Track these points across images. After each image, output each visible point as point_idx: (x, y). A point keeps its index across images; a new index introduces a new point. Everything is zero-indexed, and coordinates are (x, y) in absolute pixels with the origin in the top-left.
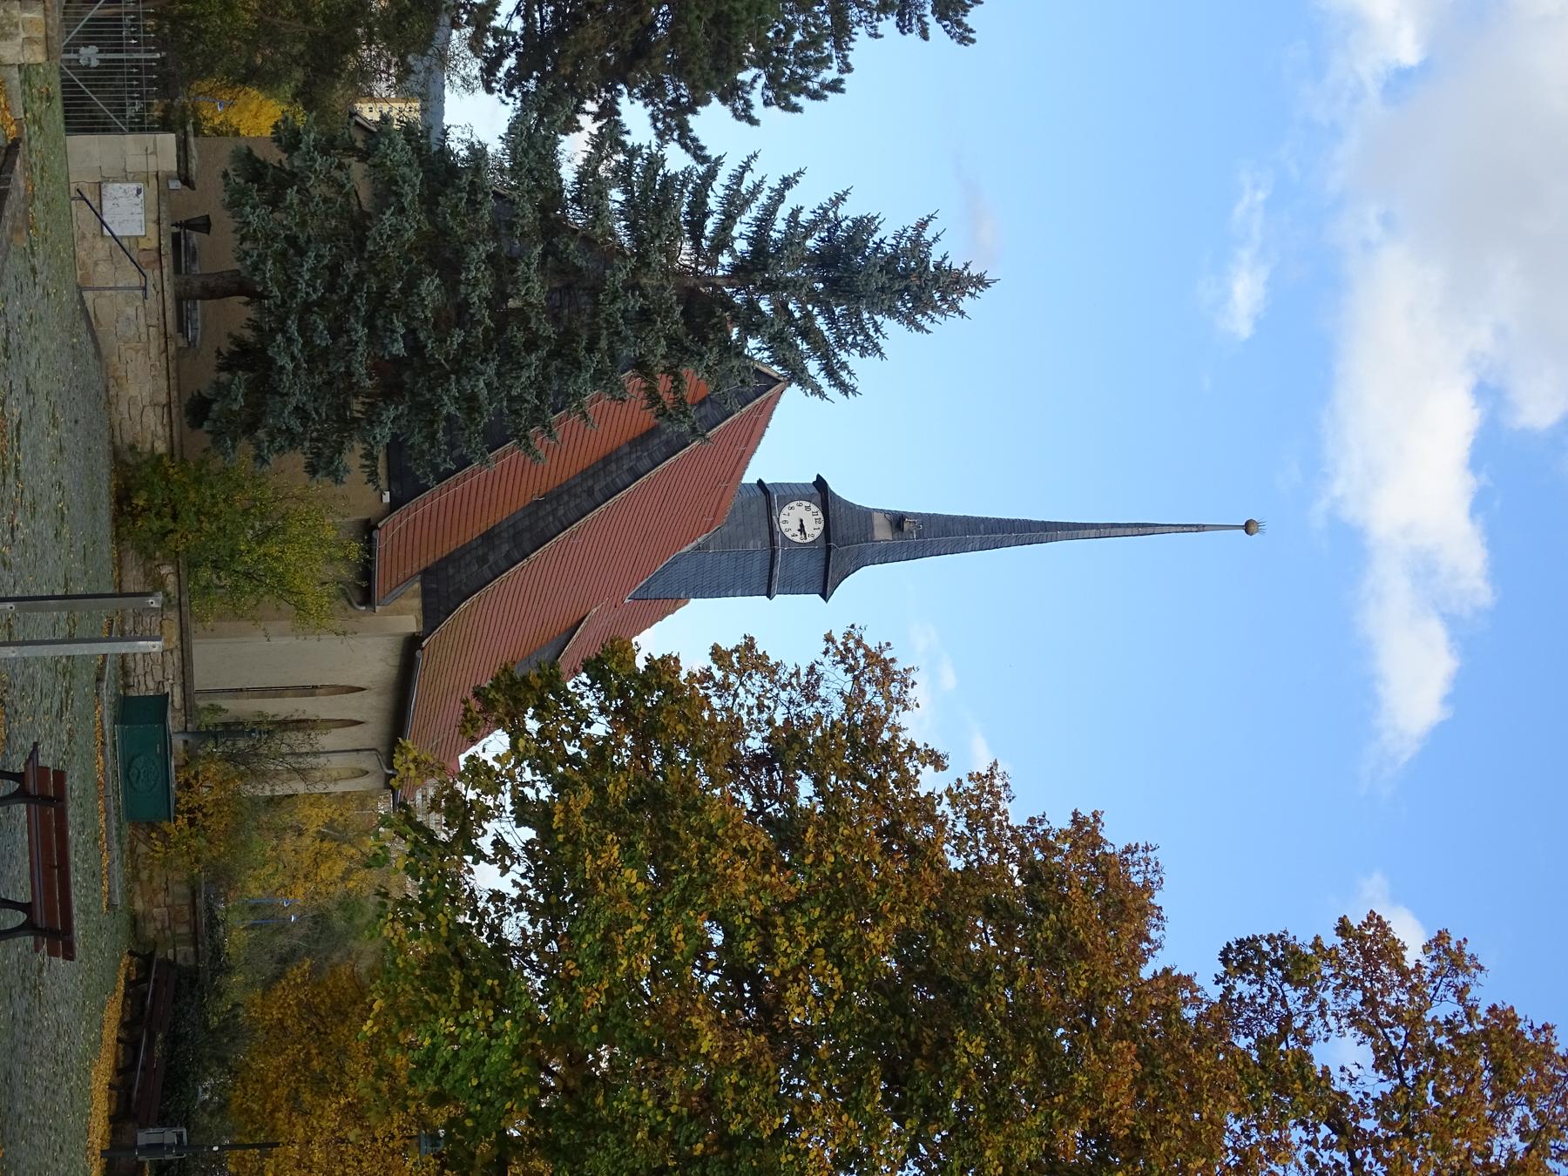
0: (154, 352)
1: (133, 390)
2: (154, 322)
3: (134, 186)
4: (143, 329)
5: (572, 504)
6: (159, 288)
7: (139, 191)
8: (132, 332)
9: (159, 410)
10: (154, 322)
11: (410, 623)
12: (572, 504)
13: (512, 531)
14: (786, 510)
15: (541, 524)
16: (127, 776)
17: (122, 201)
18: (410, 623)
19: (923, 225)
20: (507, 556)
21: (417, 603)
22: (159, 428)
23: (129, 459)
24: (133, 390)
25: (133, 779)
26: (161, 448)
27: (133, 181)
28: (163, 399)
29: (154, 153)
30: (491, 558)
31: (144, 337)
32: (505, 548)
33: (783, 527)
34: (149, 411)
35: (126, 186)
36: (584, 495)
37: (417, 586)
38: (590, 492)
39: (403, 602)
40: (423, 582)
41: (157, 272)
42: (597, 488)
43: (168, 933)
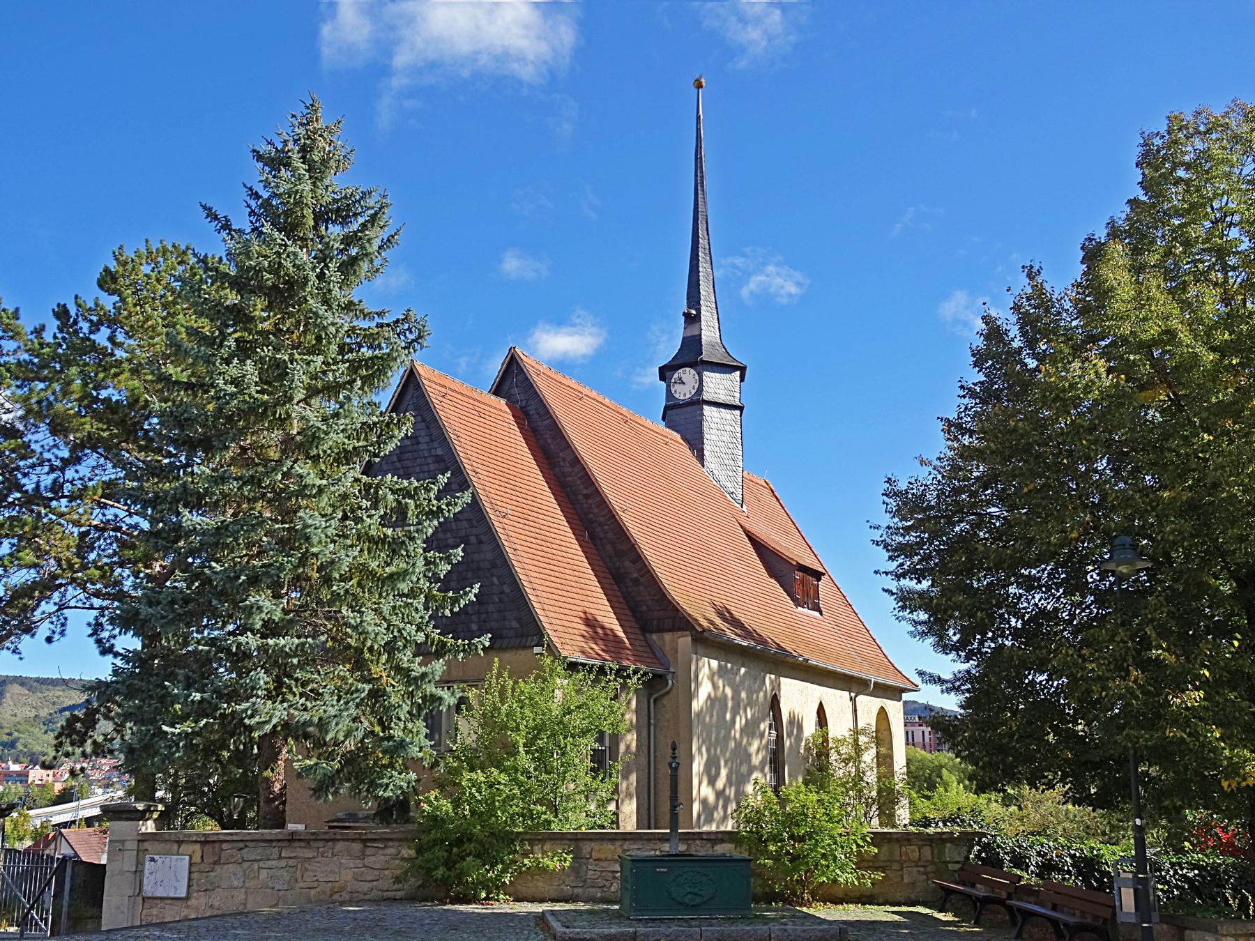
0: (309, 854)
1: (347, 876)
2: (276, 851)
3: (147, 864)
4: (283, 863)
5: (596, 511)
6: (241, 845)
7: (152, 860)
8: (285, 874)
9: (369, 851)
10: (276, 851)
11: (685, 641)
12: (596, 511)
13: (615, 559)
14: (677, 396)
15: (610, 535)
16: (694, 908)
17: (159, 877)
18: (685, 641)
19: (259, 157)
20: (634, 562)
21: (668, 637)
22: (388, 851)
23: (413, 882)
24: (347, 876)
25: (698, 900)
26: (408, 852)
27: (143, 864)
28: (357, 846)
29: (123, 842)
30: (635, 575)
31: (291, 862)
32: (627, 564)
33: (688, 396)
34: (369, 861)
35: (147, 872)
36: (590, 501)
37: (654, 637)
38: (587, 497)
39: (667, 648)
40: (651, 632)
41: (224, 846)
42: (585, 492)
43: (930, 869)
